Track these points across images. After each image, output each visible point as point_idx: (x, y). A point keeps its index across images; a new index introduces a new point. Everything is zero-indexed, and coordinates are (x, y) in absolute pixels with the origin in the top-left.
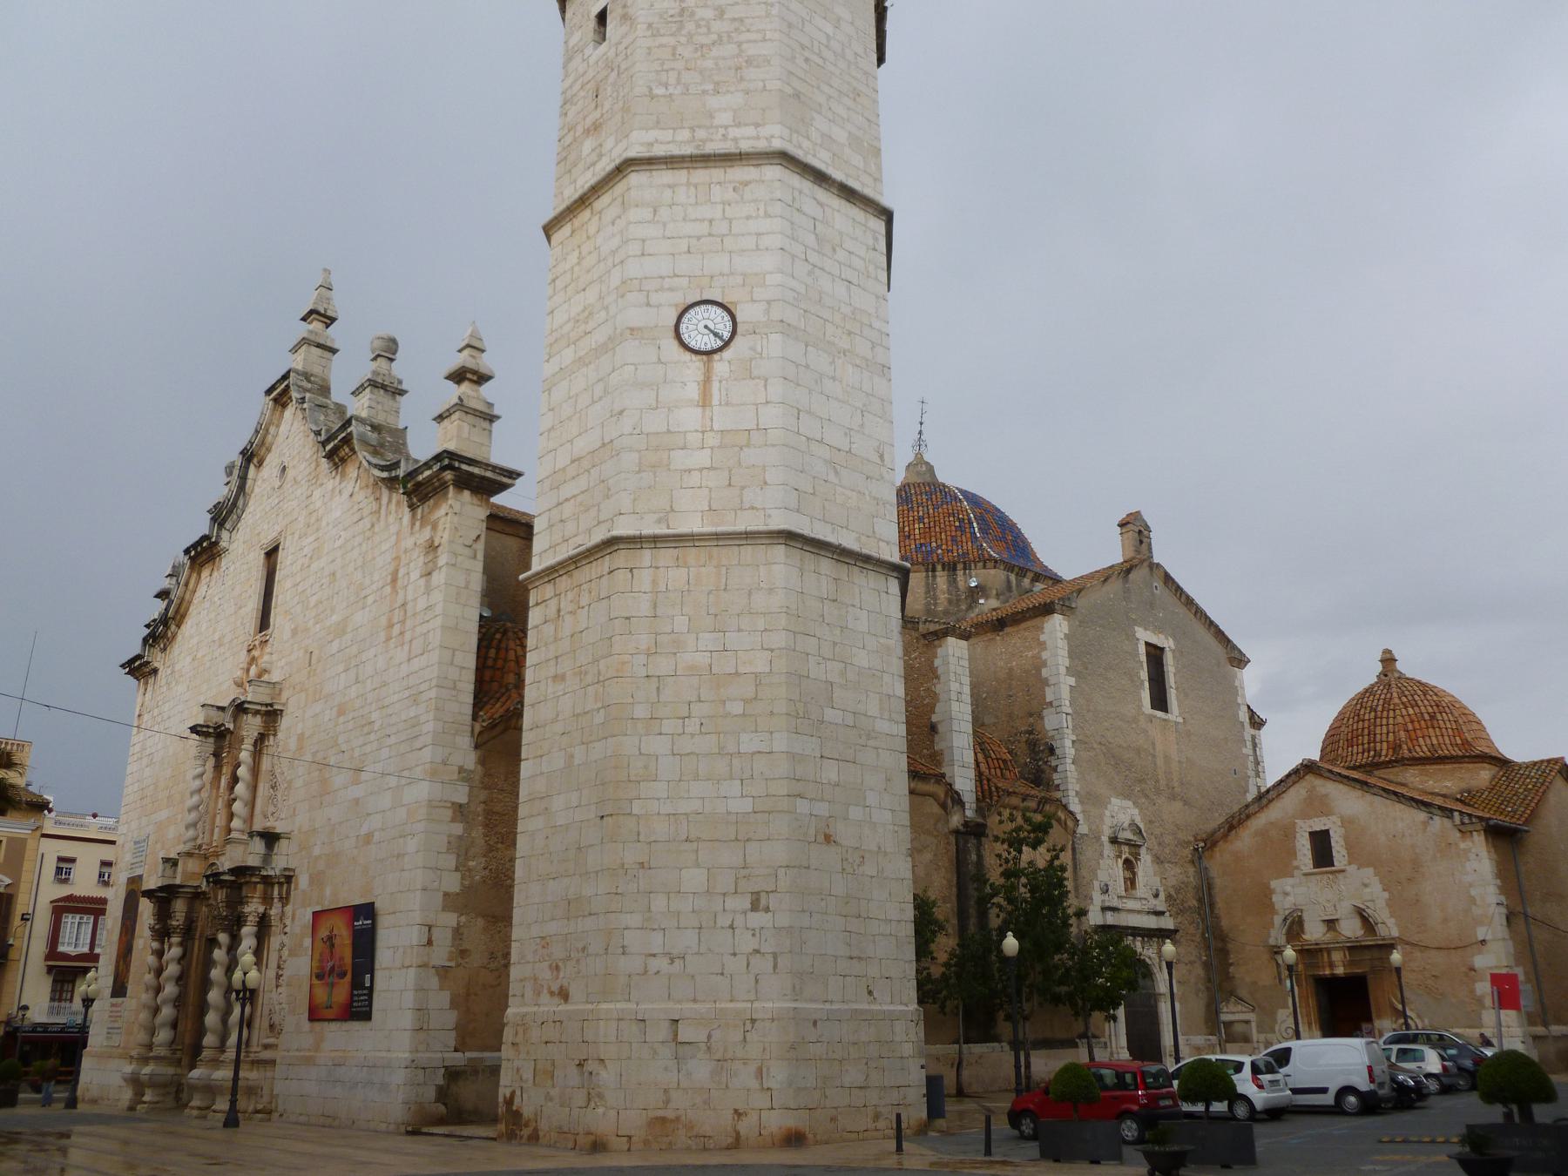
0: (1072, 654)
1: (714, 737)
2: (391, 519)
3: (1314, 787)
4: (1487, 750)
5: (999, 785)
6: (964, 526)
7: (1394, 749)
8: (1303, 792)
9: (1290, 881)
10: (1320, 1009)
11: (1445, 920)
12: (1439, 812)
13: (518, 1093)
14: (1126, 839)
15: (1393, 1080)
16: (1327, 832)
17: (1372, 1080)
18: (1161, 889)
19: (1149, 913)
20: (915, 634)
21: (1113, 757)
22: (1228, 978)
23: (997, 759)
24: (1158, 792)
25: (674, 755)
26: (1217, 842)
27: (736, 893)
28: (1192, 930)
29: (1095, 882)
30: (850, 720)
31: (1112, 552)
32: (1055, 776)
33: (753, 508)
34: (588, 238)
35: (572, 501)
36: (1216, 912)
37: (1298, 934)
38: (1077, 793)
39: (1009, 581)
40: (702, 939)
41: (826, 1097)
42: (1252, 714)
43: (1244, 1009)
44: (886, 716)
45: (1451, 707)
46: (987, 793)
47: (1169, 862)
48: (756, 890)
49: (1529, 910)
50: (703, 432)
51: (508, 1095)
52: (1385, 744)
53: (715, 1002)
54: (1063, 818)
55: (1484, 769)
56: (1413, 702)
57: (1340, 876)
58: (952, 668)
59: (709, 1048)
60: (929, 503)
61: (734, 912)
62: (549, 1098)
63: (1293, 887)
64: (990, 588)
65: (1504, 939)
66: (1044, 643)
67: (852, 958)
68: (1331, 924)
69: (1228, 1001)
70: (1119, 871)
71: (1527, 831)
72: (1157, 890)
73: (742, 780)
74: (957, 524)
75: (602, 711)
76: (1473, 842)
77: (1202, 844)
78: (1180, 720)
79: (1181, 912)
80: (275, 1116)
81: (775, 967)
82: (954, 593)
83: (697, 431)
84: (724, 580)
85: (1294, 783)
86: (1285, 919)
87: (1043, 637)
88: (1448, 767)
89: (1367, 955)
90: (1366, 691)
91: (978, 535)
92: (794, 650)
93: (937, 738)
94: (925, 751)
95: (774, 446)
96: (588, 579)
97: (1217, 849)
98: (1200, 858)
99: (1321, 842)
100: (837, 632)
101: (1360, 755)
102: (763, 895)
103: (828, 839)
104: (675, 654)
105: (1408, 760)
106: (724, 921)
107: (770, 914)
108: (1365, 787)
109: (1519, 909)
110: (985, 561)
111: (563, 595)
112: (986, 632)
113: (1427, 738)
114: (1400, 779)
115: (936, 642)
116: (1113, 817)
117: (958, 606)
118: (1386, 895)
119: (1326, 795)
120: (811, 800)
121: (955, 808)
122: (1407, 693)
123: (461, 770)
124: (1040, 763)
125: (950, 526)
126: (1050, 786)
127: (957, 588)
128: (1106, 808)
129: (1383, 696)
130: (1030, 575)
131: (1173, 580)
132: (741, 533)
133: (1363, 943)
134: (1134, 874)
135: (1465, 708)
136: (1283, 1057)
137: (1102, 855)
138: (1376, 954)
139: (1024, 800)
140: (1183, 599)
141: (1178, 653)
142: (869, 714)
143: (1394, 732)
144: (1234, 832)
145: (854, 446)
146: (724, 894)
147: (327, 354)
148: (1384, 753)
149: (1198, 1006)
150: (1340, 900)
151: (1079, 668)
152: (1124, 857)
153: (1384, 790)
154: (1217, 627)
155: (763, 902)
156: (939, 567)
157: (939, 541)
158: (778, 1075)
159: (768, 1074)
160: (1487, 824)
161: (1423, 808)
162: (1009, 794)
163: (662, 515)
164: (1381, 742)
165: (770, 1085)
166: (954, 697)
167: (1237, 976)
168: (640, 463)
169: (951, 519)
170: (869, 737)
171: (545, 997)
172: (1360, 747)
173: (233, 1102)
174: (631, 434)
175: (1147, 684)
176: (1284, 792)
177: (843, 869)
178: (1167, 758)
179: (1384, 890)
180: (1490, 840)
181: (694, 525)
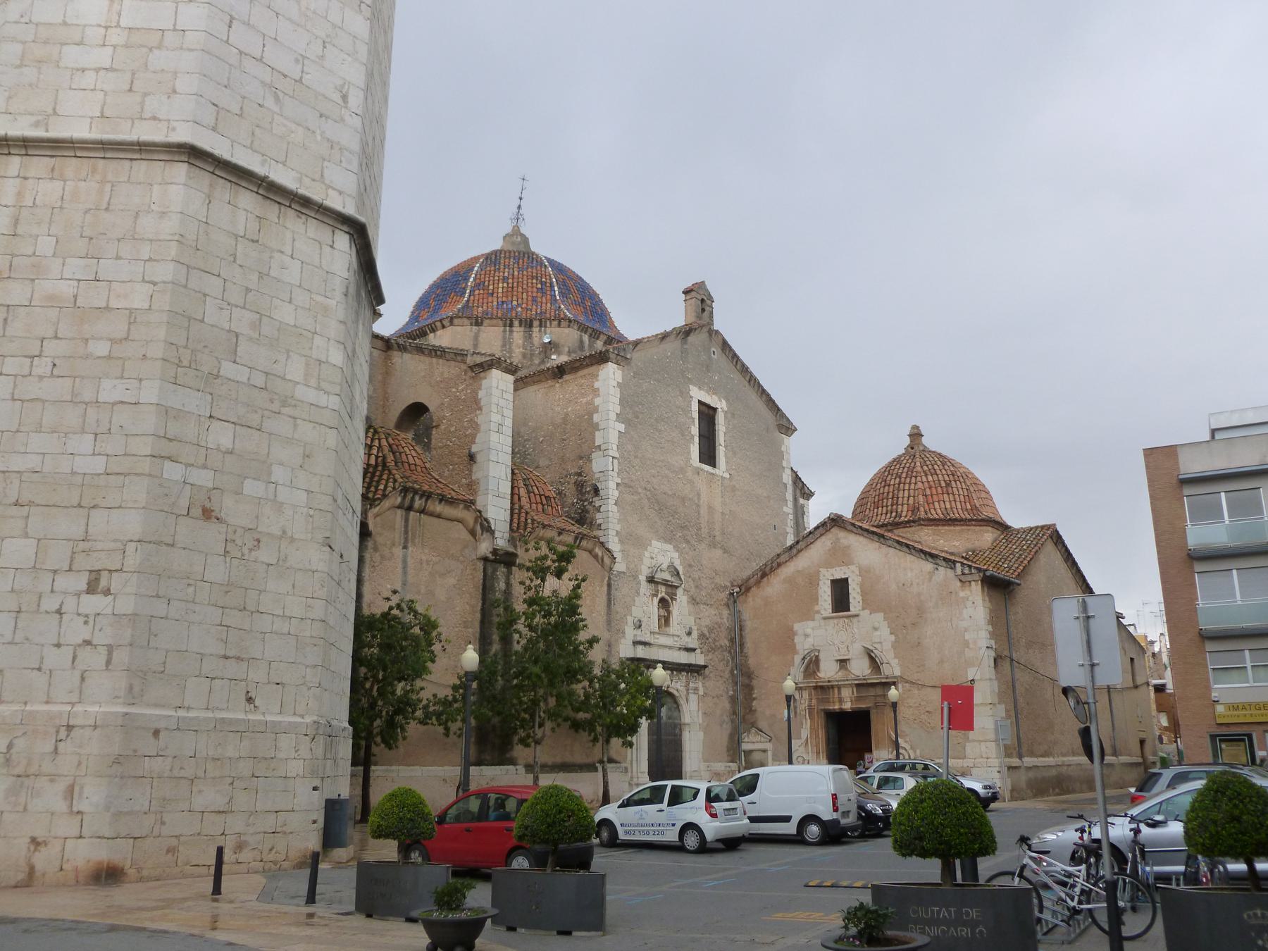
0: (623, 402)
1: (68, 382)
3: (838, 539)
4: (991, 515)
5: (535, 518)
6: (545, 288)
7: (913, 511)
8: (829, 543)
9: (811, 624)
10: (828, 741)
11: (941, 662)
12: (944, 563)
14: (663, 580)
15: (861, 808)
16: (846, 580)
17: (836, 809)
18: (694, 628)
19: (680, 649)
20: (464, 367)
21: (658, 503)
22: (751, 711)
23: (540, 495)
24: (700, 540)
25: (14, 400)
26: (750, 588)
27: (70, 570)
28: (721, 666)
29: (628, 617)
30: (259, 380)
31: (676, 315)
32: (598, 516)
33: (154, 118)
36: (745, 651)
37: (815, 672)
38: (618, 533)
39: (581, 342)
40: (19, 625)
41: (163, 823)
42: (797, 479)
43: (763, 740)
44: (313, 382)
45: (965, 477)
46: (522, 524)
47: (705, 604)
48: (97, 568)
49: (1015, 656)
50: (106, 28)
52: (905, 507)
53: (26, 703)
54: (600, 554)
55: (987, 532)
56: (932, 471)
57: (855, 620)
58: (494, 400)
59: (8, 760)
60: (516, 265)
61: (65, 593)
63: (813, 629)
64: (563, 346)
65: (990, 679)
66: (598, 389)
67: (226, 657)
68: (843, 663)
69: (749, 732)
70: (653, 609)
71: (1019, 585)
72: (690, 628)
73: (96, 434)
74: (539, 286)
76: (971, 591)
77: (738, 590)
78: (727, 475)
79: (712, 650)
81: (108, 662)
82: (529, 348)
83: (100, 26)
84: (107, 199)
85: (822, 535)
86: (804, 659)
87: (596, 385)
88: (958, 528)
89: (872, 692)
90: (894, 460)
91: (558, 298)
92: (185, 287)
93: (475, 468)
94: (464, 480)
95: (192, 50)
97: (749, 594)
98: (735, 602)
99: (840, 590)
100: (255, 277)
101: (884, 516)
102: (105, 575)
103: (207, 514)
104: (33, 280)
105: (923, 520)
106: (50, 604)
107: (110, 598)
108: (882, 539)
109: (1006, 653)
110: (560, 320)
112: (547, 380)
113: (942, 502)
114: (916, 537)
115: (482, 374)
116: (652, 558)
117: (531, 360)
118: (893, 638)
119: (848, 547)
120: (188, 465)
121: (484, 536)
122: (928, 463)
124: (585, 504)
125: (532, 287)
126: (592, 524)
127: (532, 343)
128: (646, 550)
129: (907, 465)
130: (603, 338)
131: (730, 347)
132: (131, 144)
133: (869, 681)
134: (669, 612)
135: (977, 479)
136: (750, 786)
137: (638, 593)
138: (879, 691)
139: (560, 534)
140: (738, 367)
141: (730, 415)
142: (288, 377)
143: (914, 497)
144: (765, 579)
145: (306, 77)
146: (55, 572)
148: (904, 514)
149: (722, 736)
150: (853, 642)
151: (630, 416)
152: (660, 596)
153: (898, 542)
154: (768, 395)
155: (103, 583)
156: (516, 323)
157: (520, 301)
158: (93, 796)
159: (81, 794)
160: (984, 574)
161: (930, 560)
162: (544, 526)
163: (40, 118)
164: (903, 505)
165: (81, 808)
166: (494, 427)
167: (759, 710)
168: (23, 56)
169: (534, 281)
170: (284, 403)
172: (885, 508)
174: (16, 22)
175: (697, 439)
176: (811, 543)
177: (226, 552)
178: (711, 509)
179: (891, 634)
180: (986, 589)
181: (81, 132)
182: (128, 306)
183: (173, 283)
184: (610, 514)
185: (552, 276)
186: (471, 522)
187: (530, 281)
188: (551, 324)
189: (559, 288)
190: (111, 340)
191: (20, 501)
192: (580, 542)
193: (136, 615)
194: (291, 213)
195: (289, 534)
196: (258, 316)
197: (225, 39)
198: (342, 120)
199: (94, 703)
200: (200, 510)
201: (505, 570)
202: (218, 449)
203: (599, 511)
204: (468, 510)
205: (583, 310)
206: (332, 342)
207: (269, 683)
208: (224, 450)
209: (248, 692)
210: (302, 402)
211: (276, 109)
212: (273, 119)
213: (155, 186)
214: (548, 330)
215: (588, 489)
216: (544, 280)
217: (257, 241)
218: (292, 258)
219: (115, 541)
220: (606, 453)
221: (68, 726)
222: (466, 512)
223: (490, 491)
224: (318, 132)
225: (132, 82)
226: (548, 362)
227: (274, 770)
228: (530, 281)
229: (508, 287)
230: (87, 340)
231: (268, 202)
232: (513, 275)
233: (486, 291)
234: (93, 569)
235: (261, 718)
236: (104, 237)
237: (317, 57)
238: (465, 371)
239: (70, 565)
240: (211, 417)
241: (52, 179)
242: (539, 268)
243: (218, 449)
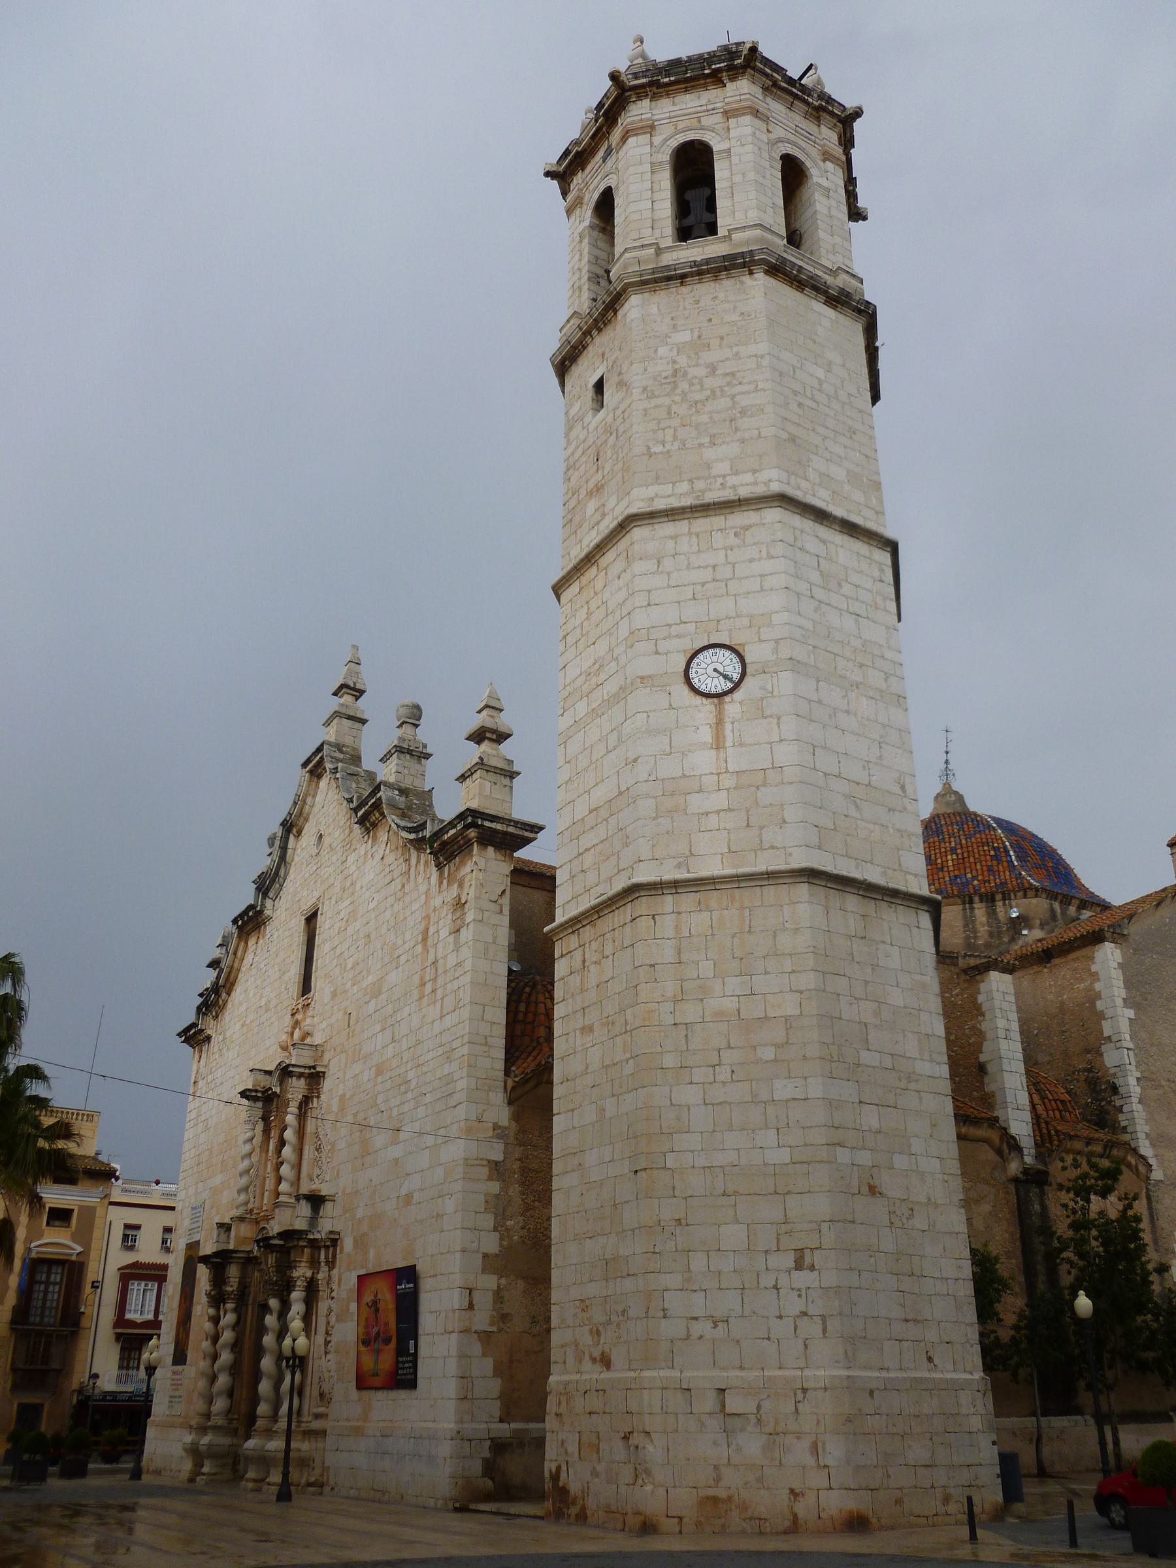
0: (1128, 985)
2: (420, 879)
5: (1059, 1128)
6: (1000, 855)
13: (564, 1468)
20: (955, 970)
23: (1055, 1101)
27: (778, 1250)
30: (888, 1062)
33: (772, 847)
34: (596, 594)
35: (592, 850)
39: (1052, 911)
44: (926, 1056)
51: (554, 1470)
54: (1133, 1162)
58: (997, 1003)
60: (961, 833)
62: (595, 1473)
66: (1097, 973)
67: (907, 1321)
73: (778, 1129)
74: (992, 853)
75: (631, 1061)
80: (327, 1489)
81: (824, 1331)
87: (1094, 968)
91: (1016, 864)
93: (986, 1080)
96: (611, 928)
100: (869, 970)
103: (873, 1190)
104: (702, 1000)
106: (768, 1280)
107: (816, 1273)
110: (1026, 890)
111: (587, 945)
112: (1032, 965)
115: (978, 977)
117: (999, 938)
120: (853, 1148)
121: (1012, 1155)
123: (496, 1126)
124: (1103, 1103)
125: (985, 855)
126: (1116, 1128)
127: (997, 919)
130: (1076, 902)
132: (762, 874)
139: (1088, 1144)
145: (873, 779)
147: (357, 725)
155: (808, 1260)
156: (976, 899)
157: (974, 873)
158: (834, 1452)
159: (824, 1450)
162: (1071, 1137)
163: (681, 860)
166: (1001, 1033)
169: (986, 848)
171: (587, 1365)
173: (286, 1475)
182: (783, 1015)
183: (816, 990)
184: (1136, 1115)
185: (1004, 839)
186: (997, 1140)
187: (981, 848)
188: (1015, 896)
189: (1015, 852)
190: (774, 1045)
191: (727, 1192)
192: (1110, 1152)
193: (840, 1287)
194: (884, 905)
195: (933, 1200)
196: (877, 1004)
197: (813, 767)
198: (905, 809)
199: (818, 1368)
200: (867, 1188)
201: (1037, 1190)
202: (870, 1131)
203: (1121, 1112)
204: (993, 1128)
205: (1045, 873)
206: (933, 1015)
207: (941, 1342)
208: (874, 1130)
209: (927, 1352)
210: (922, 1075)
211: (857, 815)
212: (857, 825)
213: (785, 907)
214: (1014, 903)
215: (1103, 1087)
216: (996, 845)
217: (865, 937)
218: (892, 946)
219: (810, 1222)
220: (1118, 1045)
221: (803, 1389)
222: (989, 1130)
223: (1009, 1105)
224: (890, 825)
225: (748, 818)
226: (1019, 938)
227: (960, 1425)
228: (981, 848)
229: (958, 859)
230: (755, 1047)
231: (867, 900)
232: (961, 844)
233: (934, 866)
234: (797, 1248)
235: (941, 1376)
236: (752, 956)
237: (877, 758)
238: (958, 974)
239: (778, 1245)
240: (860, 1102)
241: (700, 910)
242: (987, 831)
243: (870, 1131)
